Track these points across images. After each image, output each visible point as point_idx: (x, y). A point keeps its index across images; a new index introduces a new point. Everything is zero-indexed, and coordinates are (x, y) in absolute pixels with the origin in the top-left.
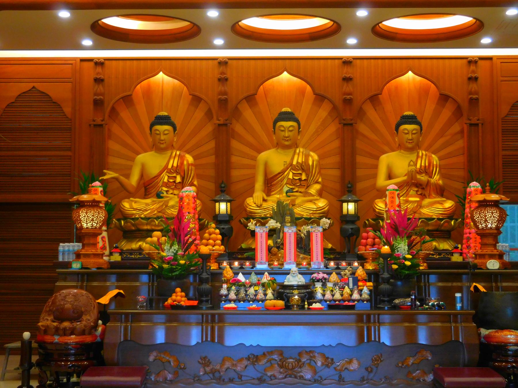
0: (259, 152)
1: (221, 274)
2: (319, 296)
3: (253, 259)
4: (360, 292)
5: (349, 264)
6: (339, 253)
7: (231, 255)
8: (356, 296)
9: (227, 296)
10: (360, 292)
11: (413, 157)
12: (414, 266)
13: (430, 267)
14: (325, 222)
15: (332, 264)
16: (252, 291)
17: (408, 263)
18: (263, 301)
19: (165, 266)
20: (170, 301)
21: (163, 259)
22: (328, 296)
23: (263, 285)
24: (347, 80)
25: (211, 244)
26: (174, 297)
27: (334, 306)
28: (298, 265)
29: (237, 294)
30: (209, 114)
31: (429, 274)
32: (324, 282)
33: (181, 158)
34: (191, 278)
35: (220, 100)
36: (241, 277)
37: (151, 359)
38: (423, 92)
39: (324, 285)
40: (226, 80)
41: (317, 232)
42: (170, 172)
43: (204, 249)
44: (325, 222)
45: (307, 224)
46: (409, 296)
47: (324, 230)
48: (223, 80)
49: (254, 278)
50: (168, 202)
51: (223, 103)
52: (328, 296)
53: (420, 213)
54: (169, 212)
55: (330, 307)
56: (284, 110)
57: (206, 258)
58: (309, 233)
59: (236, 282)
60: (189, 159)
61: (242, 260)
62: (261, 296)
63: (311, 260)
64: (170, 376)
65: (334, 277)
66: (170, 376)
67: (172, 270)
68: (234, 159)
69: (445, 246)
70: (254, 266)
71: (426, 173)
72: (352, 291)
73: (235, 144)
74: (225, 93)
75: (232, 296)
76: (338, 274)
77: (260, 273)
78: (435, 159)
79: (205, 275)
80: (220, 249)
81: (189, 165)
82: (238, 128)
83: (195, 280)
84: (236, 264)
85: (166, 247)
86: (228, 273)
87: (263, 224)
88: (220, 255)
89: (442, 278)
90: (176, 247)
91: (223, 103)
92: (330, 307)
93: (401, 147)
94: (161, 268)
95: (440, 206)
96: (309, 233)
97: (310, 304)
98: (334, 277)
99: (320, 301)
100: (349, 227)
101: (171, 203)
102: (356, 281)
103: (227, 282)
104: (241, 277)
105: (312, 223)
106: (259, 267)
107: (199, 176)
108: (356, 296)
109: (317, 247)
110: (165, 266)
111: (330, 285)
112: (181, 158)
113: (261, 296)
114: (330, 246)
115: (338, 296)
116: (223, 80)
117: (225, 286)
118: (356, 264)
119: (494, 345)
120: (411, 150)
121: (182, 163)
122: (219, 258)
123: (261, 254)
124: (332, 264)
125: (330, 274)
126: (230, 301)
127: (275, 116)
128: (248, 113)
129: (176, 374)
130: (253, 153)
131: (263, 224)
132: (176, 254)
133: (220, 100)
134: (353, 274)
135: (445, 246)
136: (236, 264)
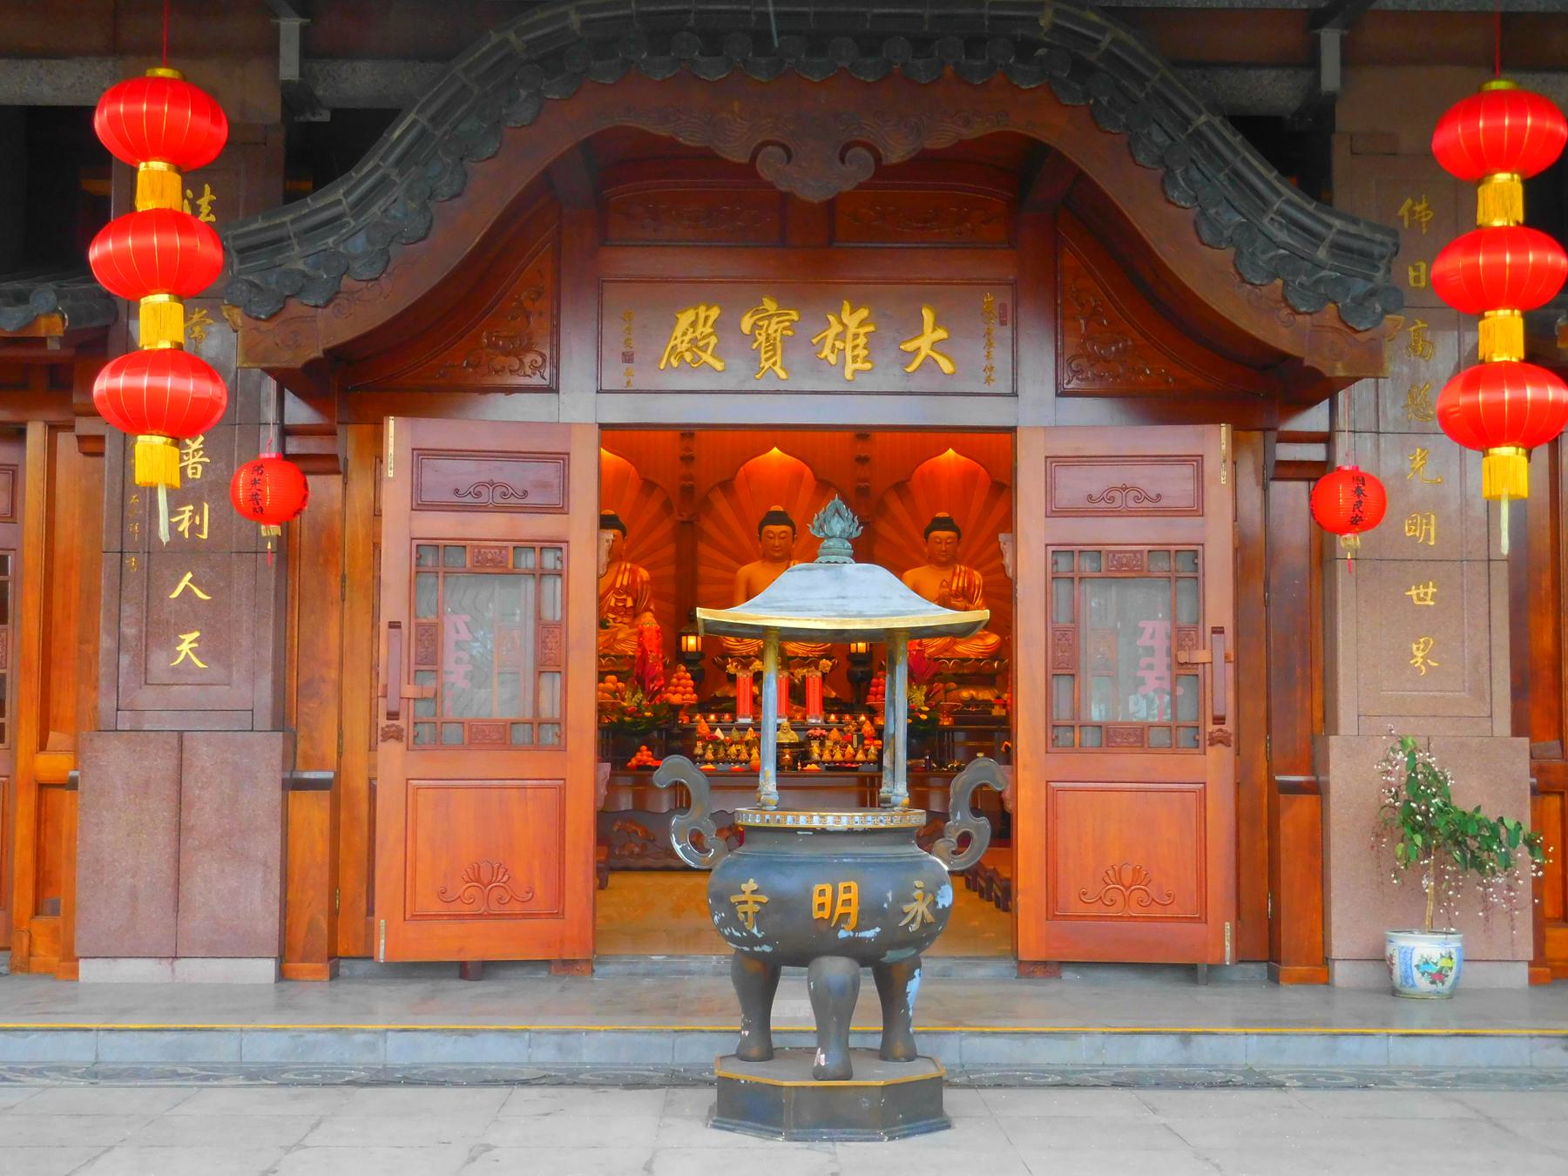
0: (744, 563)
1: (694, 729)
2: (816, 756)
3: (734, 713)
4: (866, 752)
5: (855, 719)
6: (845, 704)
7: (704, 707)
8: (860, 756)
9: (702, 756)
10: (866, 752)
11: (947, 575)
12: (932, 721)
13: (956, 722)
14: (826, 664)
15: (833, 717)
16: (733, 750)
17: (924, 717)
18: (747, 762)
19: (627, 719)
20: (634, 762)
21: (624, 711)
22: (827, 756)
23: (747, 743)
24: (862, 460)
25: (682, 692)
26: (638, 755)
27: (834, 768)
28: (790, 719)
29: (715, 753)
30: (667, 507)
31: (953, 731)
32: (822, 740)
33: (633, 572)
34: (655, 734)
35: (683, 488)
36: (718, 733)
37: (616, 828)
38: (969, 478)
39: (822, 744)
40: (692, 458)
41: (814, 676)
42: (617, 592)
43: (676, 699)
44: (826, 664)
45: (803, 666)
46: (923, 757)
47: (824, 675)
48: (688, 460)
49: (735, 735)
50: (616, 634)
51: (688, 492)
52: (827, 756)
53: (954, 651)
54: (618, 647)
55: (828, 769)
56: (774, 508)
57: (675, 709)
58: (804, 677)
59: (714, 740)
60: (644, 574)
61: (720, 713)
62: (744, 756)
63: (807, 712)
64: (637, 850)
65: (835, 734)
66: (637, 850)
67: (634, 724)
68: (703, 571)
69: (985, 695)
70: (735, 720)
71: (965, 596)
72: (856, 751)
73: (704, 549)
74: (691, 478)
75: (709, 755)
76: (840, 730)
77: (744, 728)
78: (978, 578)
79: (676, 731)
80: (692, 698)
81: (643, 582)
82: (708, 525)
83: (660, 737)
84: (712, 717)
85: (628, 695)
86: (703, 728)
87: (746, 666)
88: (691, 706)
89: (971, 735)
90: (640, 695)
91: (688, 492)
92: (828, 769)
93: (933, 560)
94: (621, 722)
95: (979, 642)
96: (804, 677)
97: (804, 765)
98: (835, 734)
99: (817, 763)
100: (860, 669)
101: (621, 636)
102: (861, 739)
103: (702, 739)
104: (718, 733)
105: (809, 665)
106: (741, 721)
107: (656, 596)
108: (860, 756)
109: (814, 698)
110: (627, 719)
111: (829, 743)
112: (633, 572)
113: (744, 756)
114: (834, 694)
115: (838, 757)
116: (688, 460)
117: (699, 744)
118: (863, 718)
119: (128, 333)
120: (944, 565)
121: (634, 581)
122: (691, 709)
123: (744, 704)
124: (833, 717)
125: (829, 730)
126: (706, 762)
127: (762, 515)
128: (722, 506)
129: (644, 847)
130: (734, 564)
131: (746, 666)
132: (639, 704)
133: (683, 488)
134: (858, 730)
135: (985, 695)
136: (712, 717)
